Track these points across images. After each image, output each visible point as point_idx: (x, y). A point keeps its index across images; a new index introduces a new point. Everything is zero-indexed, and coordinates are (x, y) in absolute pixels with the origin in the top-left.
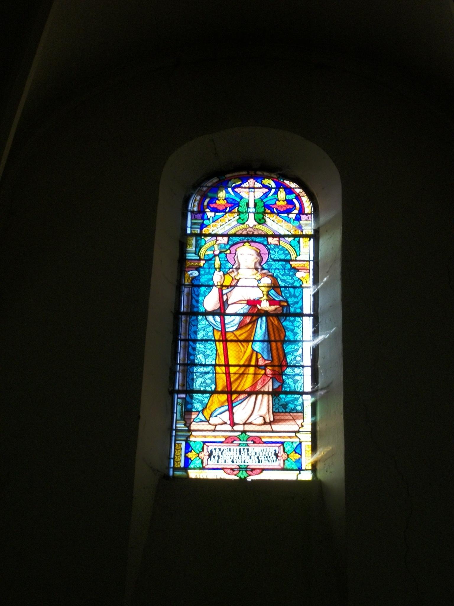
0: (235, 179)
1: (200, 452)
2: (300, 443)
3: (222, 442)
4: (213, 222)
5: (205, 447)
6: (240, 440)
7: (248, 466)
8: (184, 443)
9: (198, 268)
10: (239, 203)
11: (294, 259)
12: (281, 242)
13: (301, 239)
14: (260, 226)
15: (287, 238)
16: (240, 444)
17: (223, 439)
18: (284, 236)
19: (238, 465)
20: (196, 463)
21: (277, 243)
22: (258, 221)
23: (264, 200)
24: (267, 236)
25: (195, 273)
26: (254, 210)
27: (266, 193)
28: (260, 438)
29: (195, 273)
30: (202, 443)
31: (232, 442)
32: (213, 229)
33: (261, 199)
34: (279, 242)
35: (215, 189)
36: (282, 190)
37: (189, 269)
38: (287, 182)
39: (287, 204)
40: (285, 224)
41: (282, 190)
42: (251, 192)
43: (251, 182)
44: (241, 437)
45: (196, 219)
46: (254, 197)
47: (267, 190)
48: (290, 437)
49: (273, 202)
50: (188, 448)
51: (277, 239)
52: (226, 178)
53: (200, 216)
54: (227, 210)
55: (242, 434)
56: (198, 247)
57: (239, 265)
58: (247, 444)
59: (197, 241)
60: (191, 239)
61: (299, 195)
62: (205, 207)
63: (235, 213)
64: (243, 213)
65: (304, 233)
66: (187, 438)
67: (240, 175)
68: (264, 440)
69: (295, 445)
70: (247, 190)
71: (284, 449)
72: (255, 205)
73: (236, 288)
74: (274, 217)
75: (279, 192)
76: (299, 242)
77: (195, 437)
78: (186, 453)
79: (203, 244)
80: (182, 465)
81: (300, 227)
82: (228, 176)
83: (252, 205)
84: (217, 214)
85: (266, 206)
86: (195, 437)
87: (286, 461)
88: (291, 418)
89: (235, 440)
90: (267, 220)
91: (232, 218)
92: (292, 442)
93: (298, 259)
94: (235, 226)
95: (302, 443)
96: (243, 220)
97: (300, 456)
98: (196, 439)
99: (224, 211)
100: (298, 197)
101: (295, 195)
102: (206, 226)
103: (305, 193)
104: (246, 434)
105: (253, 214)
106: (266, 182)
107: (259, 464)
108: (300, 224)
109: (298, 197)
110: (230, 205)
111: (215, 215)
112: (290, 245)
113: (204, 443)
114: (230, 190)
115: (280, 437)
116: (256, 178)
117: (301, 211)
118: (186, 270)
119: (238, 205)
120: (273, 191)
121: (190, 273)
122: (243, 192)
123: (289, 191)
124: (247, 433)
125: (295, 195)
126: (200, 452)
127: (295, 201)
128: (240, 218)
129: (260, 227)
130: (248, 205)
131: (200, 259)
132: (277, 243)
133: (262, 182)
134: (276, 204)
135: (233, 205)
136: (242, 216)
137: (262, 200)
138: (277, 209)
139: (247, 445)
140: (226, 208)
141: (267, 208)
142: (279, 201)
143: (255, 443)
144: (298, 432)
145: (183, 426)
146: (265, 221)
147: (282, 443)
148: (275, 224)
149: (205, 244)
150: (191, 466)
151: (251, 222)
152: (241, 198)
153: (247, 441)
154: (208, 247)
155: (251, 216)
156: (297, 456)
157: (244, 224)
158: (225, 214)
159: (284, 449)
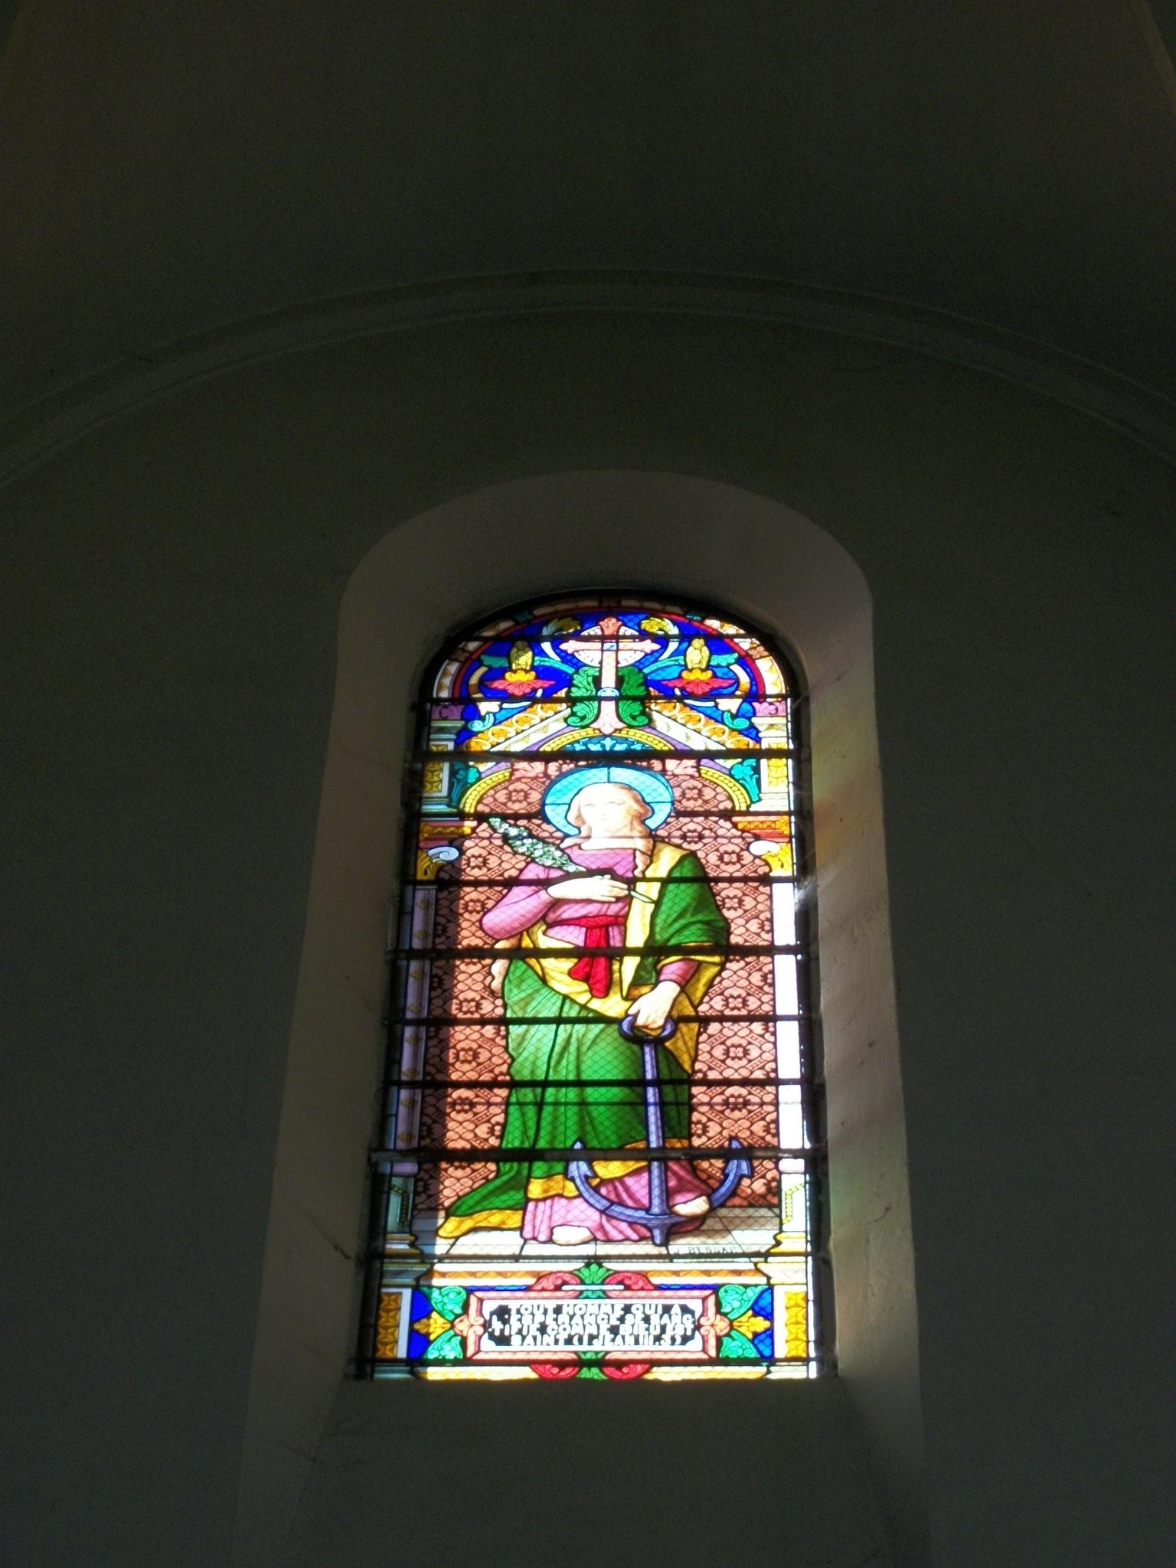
0: (561, 618)
1: (457, 1316)
2: (770, 1288)
3: (528, 1289)
4: (494, 724)
5: (473, 1300)
6: (583, 1283)
7: (607, 1353)
8: (407, 1295)
9: (456, 841)
10: (571, 678)
11: (744, 808)
12: (704, 770)
13: (764, 762)
14: (632, 731)
15: (720, 761)
16: (581, 1292)
17: (531, 1281)
18: (711, 755)
19: (576, 1353)
20: (443, 1347)
21: (692, 771)
22: (629, 720)
23: (646, 671)
24: (662, 756)
25: (450, 854)
26: (616, 693)
27: (653, 652)
28: (643, 1275)
29: (450, 854)
30: (464, 1294)
31: (558, 1288)
32: (494, 740)
33: (638, 666)
34: (699, 771)
35: (503, 646)
36: (698, 643)
37: (431, 844)
38: (714, 624)
39: (538, 677)
40: (708, 727)
41: (698, 643)
42: (604, 655)
43: (610, 625)
44: (585, 1273)
45: (445, 719)
46: (618, 662)
47: (656, 647)
48: (738, 1273)
49: (674, 673)
50: (422, 1308)
51: (692, 762)
52: (535, 617)
53: (457, 710)
54: (539, 693)
55: (588, 1265)
56: (459, 785)
57: (590, 829)
58: (604, 1292)
59: (453, 774)
60: (437, 767)
61: (750, 656)
62: (471, 690)
63: (559, 701)
64: (581, 700)
65: (764, 745)
66: (418, 1279)
67: (578, 608)
68: (656, 1280)
69: (752, 1294)
70: (598, 645)
71: (718, 1305)
72: (620, 682)
73: (664, 875)
74: (677, 710)
75: (691, 649)
76: (757, 770)
77: (443, 1275)
78: (414, 1318)
79: (471, 779)
80: (402, 1352)
81: (752, 732)
82: (539, 612)
83: (609, 680)
84: (505, 706)
85: (647, 683)
86: (443, 1275)
87: (725, 1340)
88: (719, 1226)
89: (565, 1283)
90: (655, 715)
91: (551, 713)
92: (746, 1286)
93: (753, 808)
94: (558, 734)
95: (776, 1288)
96: (583, 718)
97: (767, 1324)
98: (447, 1282)
99: (530, 698)
100: (746, 661)
101: (736, 655)
102: (475, 734)
103: (766, 649)
104: (600, 1266)
105: (612, 704)
106: (652, 625)
107: (637, 1348)
108: (752, 726)
109: (746, 661)
110: (547, 684)
111: (501, 709)
112: (732, 776)
113: (470, 1291)
114: (546, 646)
115: (707, 1273)
116: (622, 614)
117: (755, 694)
118: (422, 845)
119: (567, 681)
120: (673, 646)
121: (431, 852)
122: (588, 652)
123: (718, 644)
124: (607, 1265)
125: (736, 655)
126: (457, 1316)
127: (737, 669)
128: (573, 714)
129: (634, 735)
130: (597, 681)
131: (463, 816)
132: (692, 771)
133: (639, 625)
134: (680, 677)
135: (554, 684)
136: (579, 708)
137: (640, 670)
138: (682, 689)
139: (606, 1295)
140: (535, 690)
141: (646, 690)
142: (690, 671)
143: (628, 1288)
144: (766, 1255)
145: (406, 1247)
146: (651, 720)
147: (715, 1289)
148: (674, 725)
149: (479, 779)
150: (432, 1354)
151: (608, 719)
152: (578, 665)
153: (602, 1283)
154: (485, 785)
155: (608, 708)
156: (761, 1324)
157: (587, 726)
158: (530, 706)
159: (718, 1305)
